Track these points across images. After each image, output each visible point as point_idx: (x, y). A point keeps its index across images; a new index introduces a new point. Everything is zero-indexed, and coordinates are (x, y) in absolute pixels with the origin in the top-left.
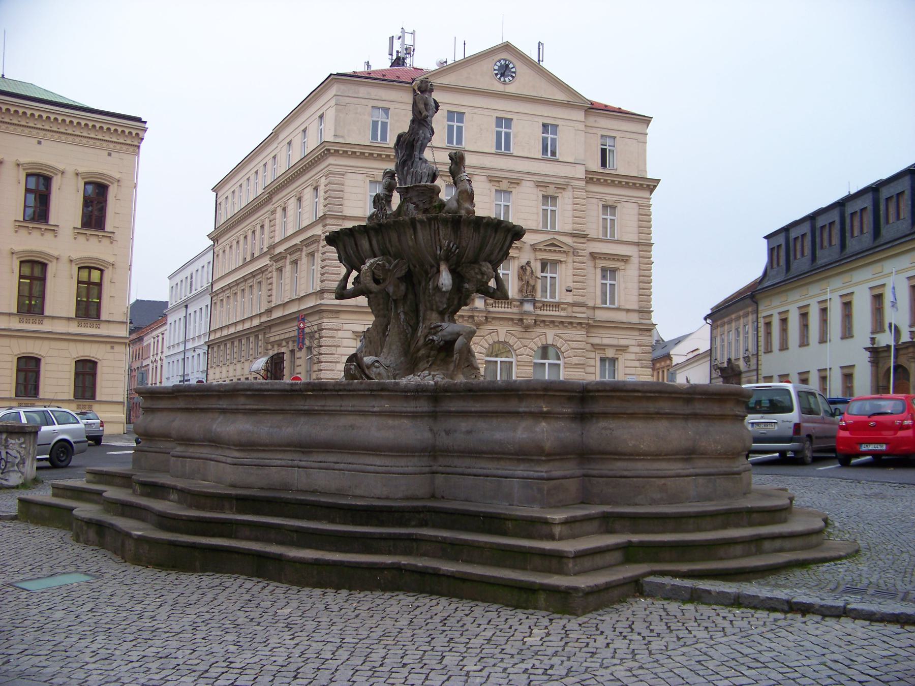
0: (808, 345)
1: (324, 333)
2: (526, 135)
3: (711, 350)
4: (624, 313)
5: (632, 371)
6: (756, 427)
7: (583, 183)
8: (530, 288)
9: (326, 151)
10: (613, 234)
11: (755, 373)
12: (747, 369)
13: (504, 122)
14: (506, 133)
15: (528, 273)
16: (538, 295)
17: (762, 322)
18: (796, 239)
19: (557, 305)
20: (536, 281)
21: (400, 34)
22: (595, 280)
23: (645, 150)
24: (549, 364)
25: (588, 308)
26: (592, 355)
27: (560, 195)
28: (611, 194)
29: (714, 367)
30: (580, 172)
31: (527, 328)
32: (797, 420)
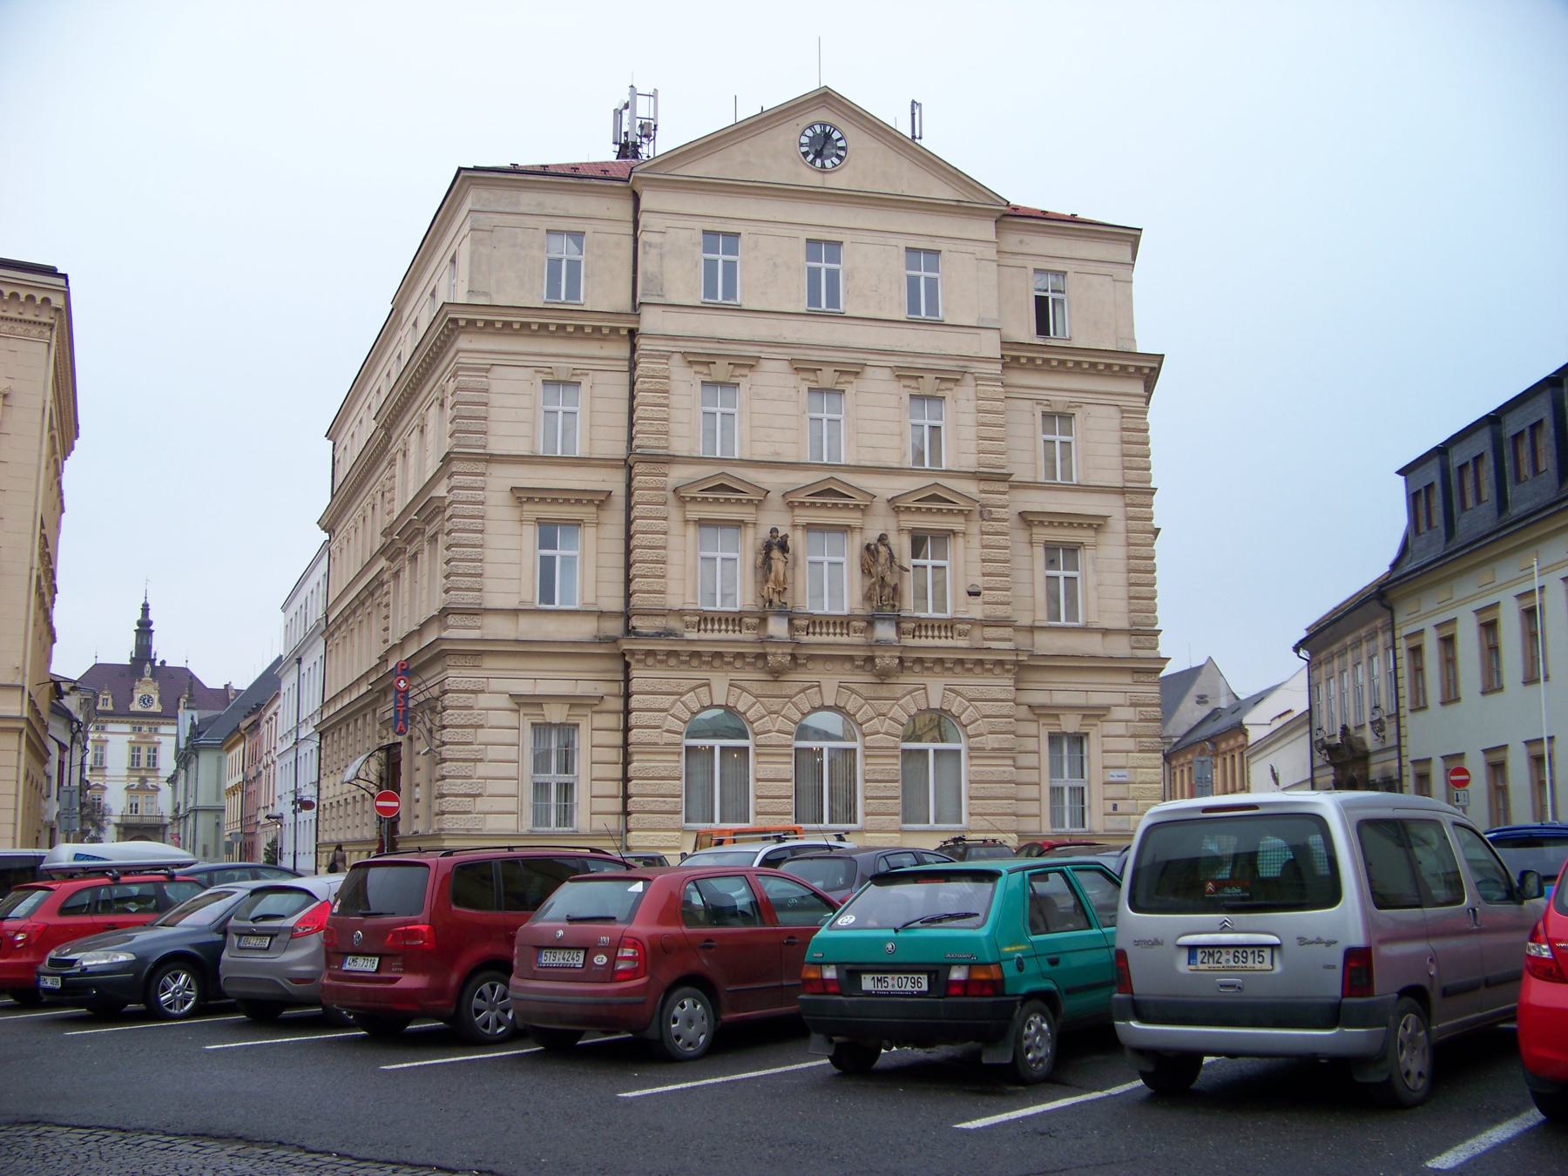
0: (1501, 689)
1: (449, 699)
2: (873, 271)
3: (1310, 710)
4: (1098, 638)
5: (1120, 759)
6: (1203, 964)
7: (996, 368)
8: (887, 591)
9: (451, 325)
10: (1067, 472)
11: (1394, 754)
12: (1379, 746)
13: (823, 248)
14: (828, 271)
15: (882, 560)
16: (909, 606)
17: (1403, 646)
18: (1462, 468)
19: (949, 626)
20: (901, 578)
21: (627, 99)
22: (1031, 571)
23: (1129, 298)
24: (723, 749)
25: (1018, 629)
26: (1031, 728)
27: (948, 395)
28: (1061, 388)
29: (1317, 746)
30: (989, 346)
31: (883, 676)
32: (1356, 937)
